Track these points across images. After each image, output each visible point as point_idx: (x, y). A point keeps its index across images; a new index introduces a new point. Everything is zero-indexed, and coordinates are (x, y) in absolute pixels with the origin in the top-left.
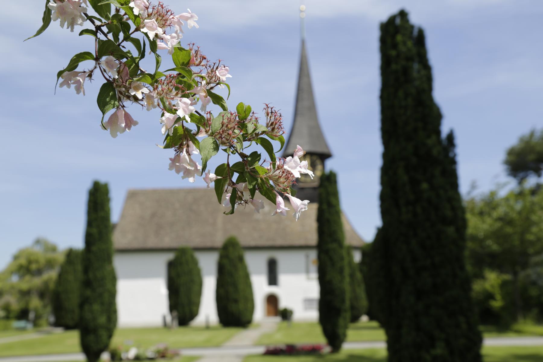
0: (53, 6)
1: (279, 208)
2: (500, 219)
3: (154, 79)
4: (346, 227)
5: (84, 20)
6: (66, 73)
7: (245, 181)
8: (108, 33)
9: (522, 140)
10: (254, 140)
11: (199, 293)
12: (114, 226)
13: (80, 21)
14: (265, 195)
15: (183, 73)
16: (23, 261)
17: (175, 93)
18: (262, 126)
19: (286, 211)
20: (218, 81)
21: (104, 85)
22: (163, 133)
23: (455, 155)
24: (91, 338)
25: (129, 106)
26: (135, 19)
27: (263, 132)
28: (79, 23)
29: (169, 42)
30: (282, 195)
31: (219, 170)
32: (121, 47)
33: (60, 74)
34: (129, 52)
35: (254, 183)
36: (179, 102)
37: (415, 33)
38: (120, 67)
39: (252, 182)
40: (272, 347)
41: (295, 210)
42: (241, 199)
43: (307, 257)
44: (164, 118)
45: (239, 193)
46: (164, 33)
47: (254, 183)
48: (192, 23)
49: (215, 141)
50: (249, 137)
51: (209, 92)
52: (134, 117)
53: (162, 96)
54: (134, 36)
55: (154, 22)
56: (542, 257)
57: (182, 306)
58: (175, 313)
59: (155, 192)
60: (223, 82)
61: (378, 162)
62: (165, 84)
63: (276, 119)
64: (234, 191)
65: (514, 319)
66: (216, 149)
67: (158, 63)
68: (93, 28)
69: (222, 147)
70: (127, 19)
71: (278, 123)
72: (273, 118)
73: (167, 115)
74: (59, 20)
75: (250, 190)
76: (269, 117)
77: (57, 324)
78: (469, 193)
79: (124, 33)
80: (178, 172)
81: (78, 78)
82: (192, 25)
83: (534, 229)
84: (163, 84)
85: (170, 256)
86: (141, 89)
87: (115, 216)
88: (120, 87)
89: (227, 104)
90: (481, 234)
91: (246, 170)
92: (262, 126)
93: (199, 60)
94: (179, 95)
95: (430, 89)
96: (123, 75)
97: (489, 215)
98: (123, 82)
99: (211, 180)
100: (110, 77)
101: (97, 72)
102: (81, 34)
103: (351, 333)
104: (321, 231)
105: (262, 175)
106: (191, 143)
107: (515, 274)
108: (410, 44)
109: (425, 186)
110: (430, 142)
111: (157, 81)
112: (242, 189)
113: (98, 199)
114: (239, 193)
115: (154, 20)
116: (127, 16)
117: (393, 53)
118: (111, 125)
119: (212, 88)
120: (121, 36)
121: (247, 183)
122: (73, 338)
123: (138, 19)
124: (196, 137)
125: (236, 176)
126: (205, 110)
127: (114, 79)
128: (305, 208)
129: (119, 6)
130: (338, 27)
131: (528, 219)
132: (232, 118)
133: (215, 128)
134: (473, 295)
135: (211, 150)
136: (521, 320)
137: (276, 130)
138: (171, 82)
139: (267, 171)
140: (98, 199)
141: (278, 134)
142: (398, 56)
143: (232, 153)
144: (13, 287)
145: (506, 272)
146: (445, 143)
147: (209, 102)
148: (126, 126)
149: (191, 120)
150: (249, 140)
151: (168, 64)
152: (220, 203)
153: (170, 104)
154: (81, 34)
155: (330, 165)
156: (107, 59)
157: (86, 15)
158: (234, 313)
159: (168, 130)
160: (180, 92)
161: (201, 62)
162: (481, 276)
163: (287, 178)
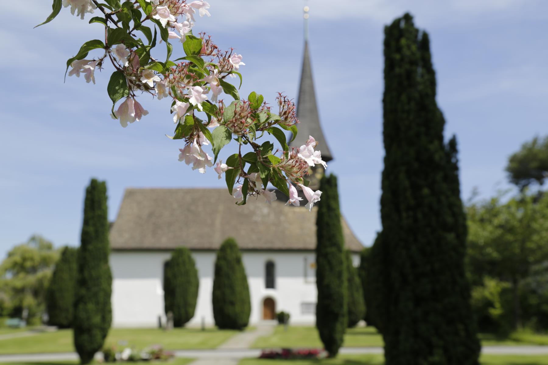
1: (293, 198)
2: (501, 226)
3: (165, 69)
4: (346, 231)
5: (94, 8)
7: (257, 171)
9: (524, 147)
11: (196, 295)
12: (111, 225)
13: (90, 8)
16: (17, 258)
17: (187, 81)
19: (300, 201)
20: (230, 70)
21: (114, 73)
22: (175, 121)
23: (457, 161)
24: (85, 337)
25: (140, 95)
26: (147, 6)
27: (276, 122)
28: (89, 10)
29: (181, 30)
30: (295, 185)
31: (230, 161)
32: (131, 35)
33: (69, 62)
34: (140, 40)
36: (192, 90)
37: (420, 37)
38: (130, 56)
40: (268, 351)
42: (253, 190)
43: (306, 260)
44: (175, 106)
45: (251, 183)
46: (176, 21)
48: (203, 11)
50: (261, 126)
51: (222, 82)
52: (145, 107)
53: (174, 84)
54: (145, 24)
55: (166, 9)
56: (547, 264)
57: (178, 308)
58: (171, 314)
59: (153, 191)
61: (380, 166)
62: (177, 73)
64: (246, 182)
65: (513, 328)
66: (229, 137)
67: (169, 51)
68: (103, 16)
69: (234, 136)
70: (138, 7)
71: (291, 113)
72: (286, 107)
73: (179, 103)
74: (70, 6)
76: (282, 106)
77: (50, 323)
78: (470, 199)
79: (135, 20)
80: (188, 162)
82: (204, 13)
83: (535, 238)
84: (175, 71)
85: (167, 257)
87: (112, 215)
88: (131, 75)
89: (239, 93)
90: (481, 242)
91: (258, 160)
93: (210, 50)
94: (191, 84)
96: (134, 63)
97: (490, 222)
99: (222, 169)
100: (120, 66)
101: (107, 62)
103: (348, 339)
105: (274, 164)
106: (201, 133)
107: (515, 282)
108: (414, 48)
109: (426, 191)
110: (433, 147)
111: (167, 70)
112: (254, 180)
113: (95, 197)
114: (251, 183)
115: (166, 7)
116: (138, 4)
117: (397, 56)
118: (120, 114)
119: (224, 77)
120: (132, 24)
122: (67, 337)
123: (149, 6)
124: (207, 127)
125: (247, 166)
128: (317, 199)
130: (342, 29)
131: (529, 226)
132: (245, 106)
133: (228, 117)
134: (473, 302)
136: (520, 329)
137: (289, 120)
140: (95, 197)
142: (402, 59)
143: (244, 143)
144: (6, 285)
145: (506, 280)
146: (447, 148)
148: (136, 115)
149: (204, 108)
150: (262, 130)
151: (179, 52)
152: (231, 194)
153: (181, 93)
158: (230, 316)
159: (180, 119)
160: (192, 80)
161: (212, 51)
163: (300, 168)
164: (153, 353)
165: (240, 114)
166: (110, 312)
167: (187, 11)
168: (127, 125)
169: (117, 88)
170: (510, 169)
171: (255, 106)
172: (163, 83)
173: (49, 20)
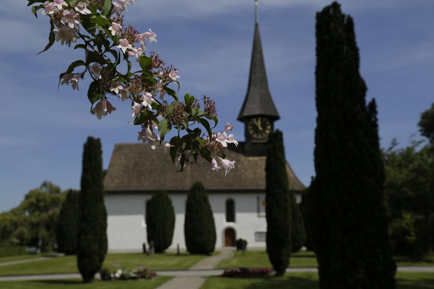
2: (414, 170)
3: (126, 77)
4: (290, 175)
5: (77, 38)
6: (65, 76)
8: (94, 45)
10: (196, 120)
13: (74, 39)
18: (201, 111)
21: (92, 84)
22: (133, 117)
23: (376, 120)
27: (202, 116)
31: (173, 141)
33: (61, 76)
34: (109, 60)
38: (102, 71)
40: (228, 271)
41: (223, 169)
43: (258, 198)
44: (133, 107)
51: (165, 88)
52: (113, 105)
54: (113, 48)
57: (158, 236)
60: (174, 81)
61: (314, 125)
62: (134, 83)
63: (211, 106)
66: (170, 127)
69: (173, 126)
73: (136, 104)
74: (61, 40)
75: (194, 155)
77: (59, 250)
81: (73, 79)
82: (153, 40)
85: (149, 197)
86: (118, 86)
87: (105, 166)
89: (178, 95)
90: (399, 183)
92: (201, 111)
94: (144, 90)
95: (357, 66)
99: (167, 147)
101: (87, 74)
102: (75, 48)
103: (292, 260)
104: (269, 178)
105: (201, 145)
106: (153, 121)
108: (340, 30)
118: (97, 111)
119: (167, 84)
120: (103, 48)
121: (192, 150)
124: (157, 118)
125: (184, 144)
126: (163, 99)
129: (101, 29)
135: (166, 129)
137: (211, 114)
138: (138, 81)
139: (205, 142)
140: (92, 149)
141: (213, 116)
144: (25, 220)
146: (368, 109)
147: (165, 93)
148: (107, 111)
150: (193, 120)
151: (136, 68)
154: (75, 48)
155: (277, 125)
156: (94, 64)
157: (79, 34)
158: (200, 242)
161: (159, 65)
162: (398, 216)
164: (139, 273)
167: (140, 39)
168: (101, 118)
169: (94, 93)
170: (421, 124)
171: (190, 101)
172: (125, 90)
173: (47, 48)
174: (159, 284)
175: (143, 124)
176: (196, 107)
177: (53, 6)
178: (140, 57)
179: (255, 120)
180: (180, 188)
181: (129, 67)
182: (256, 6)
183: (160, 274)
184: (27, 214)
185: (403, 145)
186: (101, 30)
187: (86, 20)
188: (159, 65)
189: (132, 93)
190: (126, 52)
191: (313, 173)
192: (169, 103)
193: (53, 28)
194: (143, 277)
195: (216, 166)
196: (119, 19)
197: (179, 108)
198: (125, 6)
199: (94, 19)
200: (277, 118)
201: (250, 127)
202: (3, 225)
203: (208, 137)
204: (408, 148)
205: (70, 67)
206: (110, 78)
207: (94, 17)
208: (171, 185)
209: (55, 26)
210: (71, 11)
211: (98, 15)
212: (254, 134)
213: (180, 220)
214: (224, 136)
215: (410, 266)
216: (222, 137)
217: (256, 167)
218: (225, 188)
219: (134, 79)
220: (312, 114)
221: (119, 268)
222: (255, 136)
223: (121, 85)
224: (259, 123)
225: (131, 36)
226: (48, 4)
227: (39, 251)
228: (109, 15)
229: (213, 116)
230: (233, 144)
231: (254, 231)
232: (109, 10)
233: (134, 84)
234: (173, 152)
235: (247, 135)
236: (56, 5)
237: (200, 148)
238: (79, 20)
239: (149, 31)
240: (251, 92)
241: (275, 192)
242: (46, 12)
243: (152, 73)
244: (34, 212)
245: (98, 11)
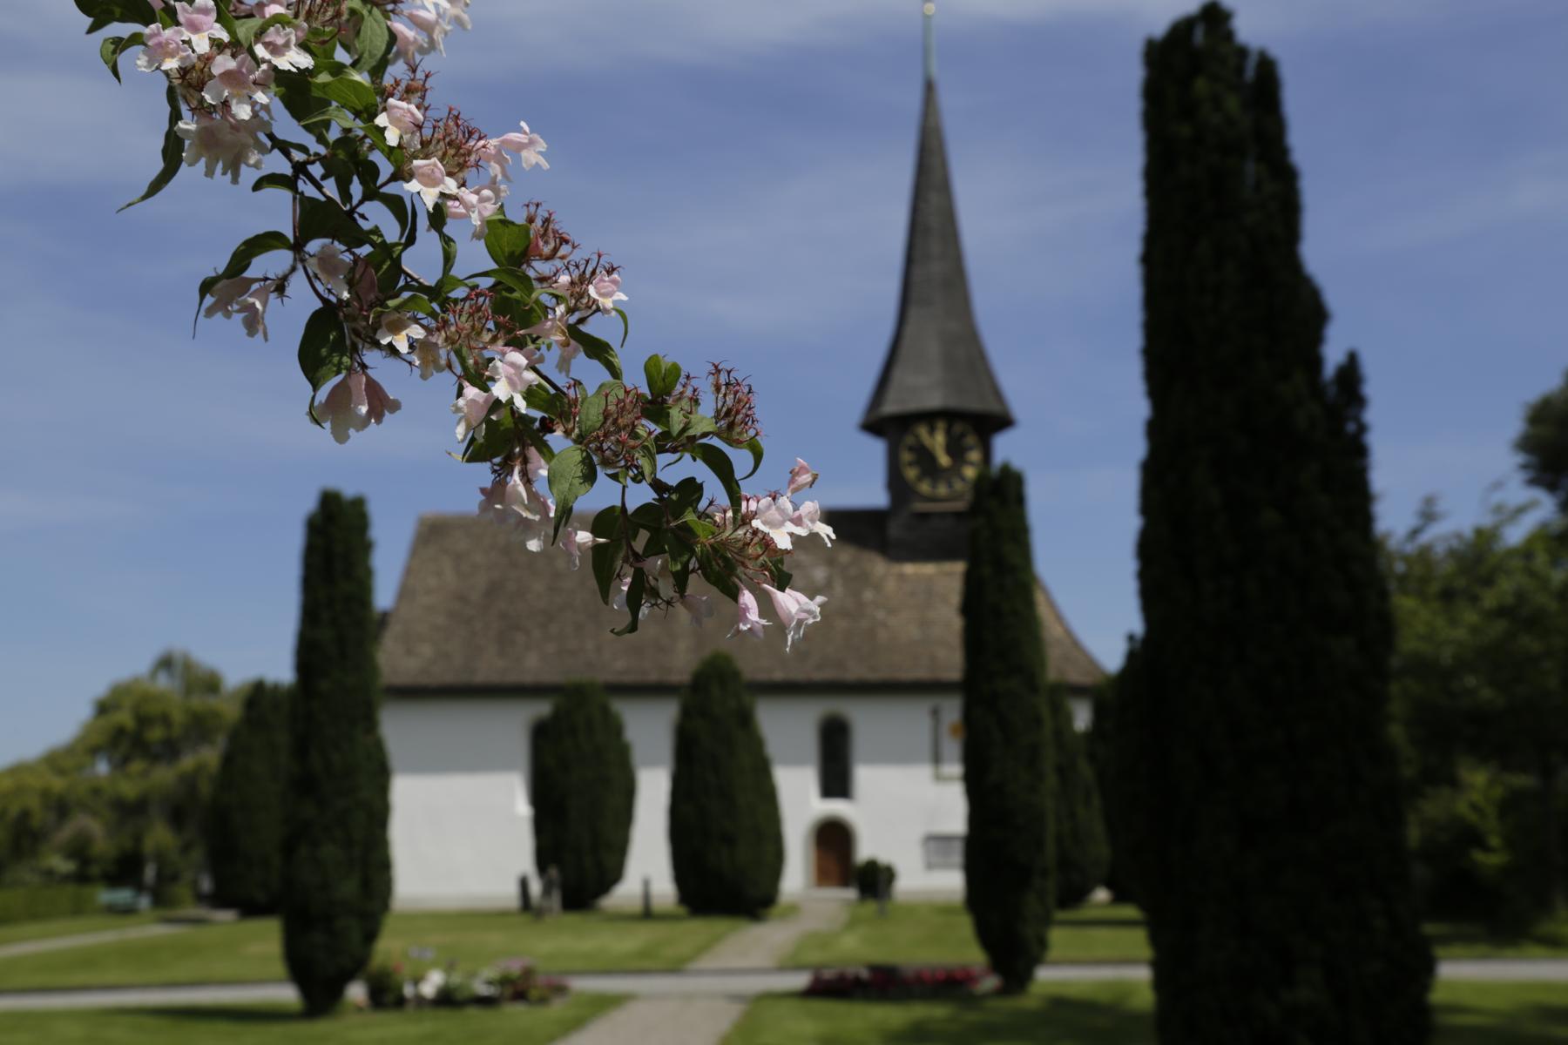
0: (187, 131)
2: (1501, 612)
5: (263, 150)
6: (219, 285)
8: (324, 177)
14: (714, 584)
15: (508, 281)
21: (316, 316)
22: (460, 437)
23: (1362, 429)
27: (705, 435)
28: (252, 161)
33: (206, 287)
35: (685, 558)
37: (1250, 73)
38: (352, 270)
39: (681, 555)
40: (828, 974)
43: (935, 713)
44: (461, 402)
47: (685, 558)
49: (589, 457)
51: (574, 332)
54: (390, 189)
57: (576, 852)
60: (606, 311)
61: (1136, 448)
63: (740, 401)
66: (590, 477)
73: (471, 392)
74: (203, 160)
75: (675, 575)
77: (219, 899)
81: (251, 300)
87: (384, 595)
90: (1447, 656)
92: (704, 419)
93: (552, 245)
94: (500, 342)
97: (1474, 599)
98: (361, 309)
99: (580, 546)
102: (257, 187)
103: (1058, 937)
104: (974, 641)
105: (705, 539)
106: (532, 452)
108: (1232, 103)
118: (333, 413)
119: (582, 321)
120: (356, 189)
122: (264, 939)
125: (643, 537)
126: (568, 371)
127: (340, 300)
137: (738, 429)
138: (479, 309)
140: (336, 536)
141: (745, 437)
143: (634, 479)
144: (96, 792)
146: (1332, 391)
147: (576, 351)
148: (370, 413)
150: (674, 450)
151: (474, 259)
152: (606, 603)
154: (257, 187)
155: (1005, 448)
157: (271, 136)
158: (725, 873)
160: (501, 334)
161: (555, 250)
162: (1442, 776)
164: (504, 981)
165: (615, 422)
166: (385, 866)
167: (489, 158)
170: (1527, 444)
172: (433, 339)
173: (156, 186)
174: (575, 1024)
175: (497, 460)
176: (685, 404)
177: (178, 39)
178: (489, 223)
179: (923, 431)
180: (653, 677)
181: (448, 259)
182: (927, 18)
183: (584, 985)
184: (102, 768)
185: (1460, 519)
186: (347, 125)
187: (296, 92)
188: (555, 250)
189: (458, 353)
190: (437, 206)
191: (1132, 620)
192: (591, 390)
193: (176, 116)
194: (520, 995)
195: (753, 616)
196: (415, 84)
197: (623, 409)
198: (438, 36)
199: (325, 85)
200: (1003, 422)
201: (906, 456)
202: (14, 810)
203: (725, 512)
204: (1479, 532)
205: (235, 255)
206: (381, 296)
207: (324, 78)
208: (620, 664)
209: (184, 108)
210: (240, 58)
211: (337, 70)
212: (920, 478)
213: (653, 791)
214: (782, 511)
215: (1484, 957)
216: (773, 514)
217: (924, 602)
218: (818, 676)
219: (464, 300)
220: (1127, 406)
221: (434, 965)
222: (925, 487)
223: (417, 321)
224: (937, 441)
225: (456, 147)
226: (158, 34)
227: (144, 902)
228: (377, 71)
229: (745, 437)
230: (814, 537)
231: (919, 831)
232: (379, 54)
233: (463, 319)
234: (601, 560)
235: (896, 483)
236: (186, 35)
237: (698, 549)
238: (273, 86)
239: (521, 130)
240: (909, 330)
241: (996, 685)
242: (150, 63)
243: (528, 278)
244: (126, 760)
245: (341, 56)
